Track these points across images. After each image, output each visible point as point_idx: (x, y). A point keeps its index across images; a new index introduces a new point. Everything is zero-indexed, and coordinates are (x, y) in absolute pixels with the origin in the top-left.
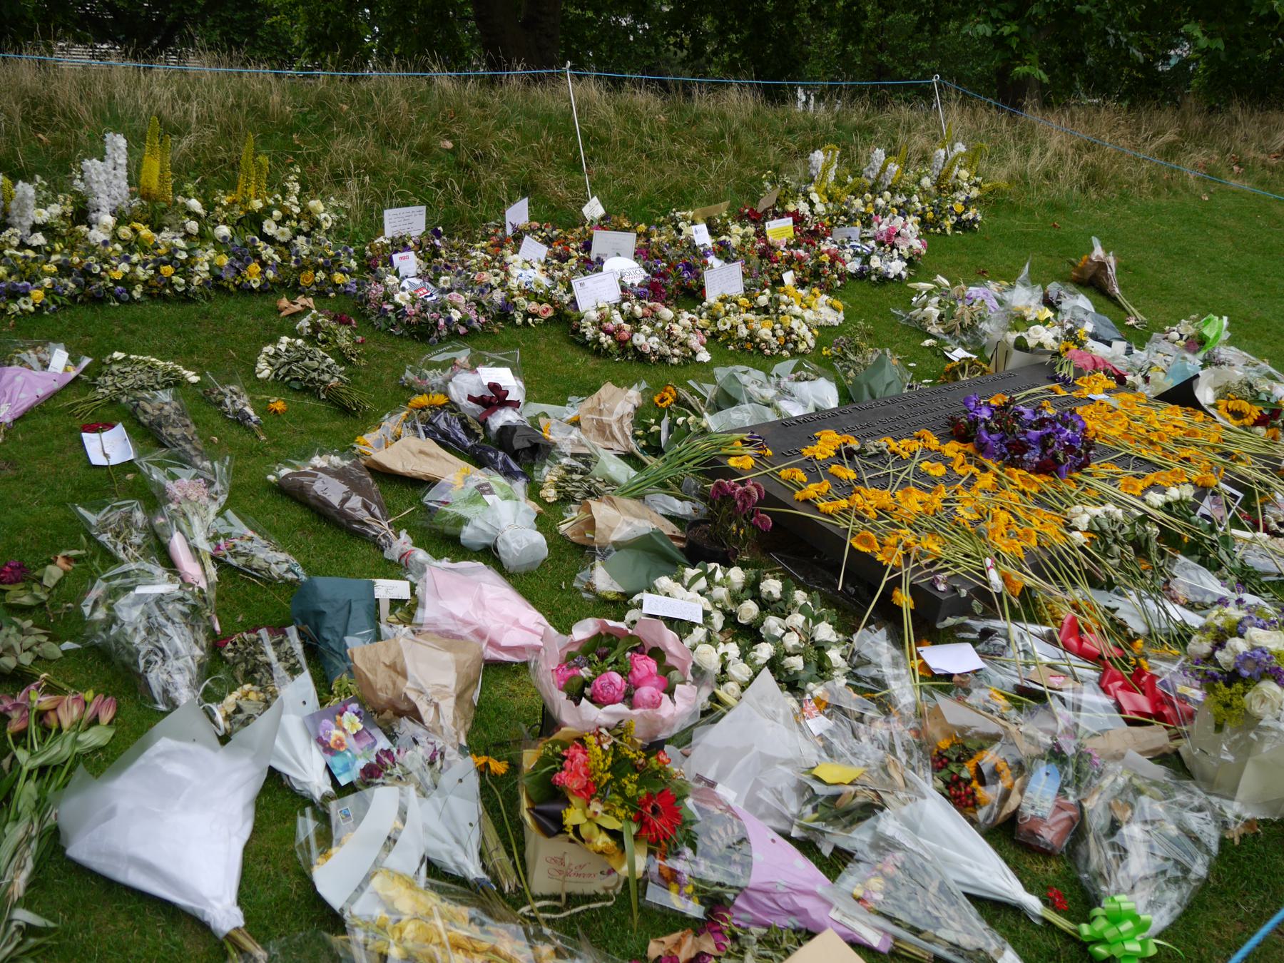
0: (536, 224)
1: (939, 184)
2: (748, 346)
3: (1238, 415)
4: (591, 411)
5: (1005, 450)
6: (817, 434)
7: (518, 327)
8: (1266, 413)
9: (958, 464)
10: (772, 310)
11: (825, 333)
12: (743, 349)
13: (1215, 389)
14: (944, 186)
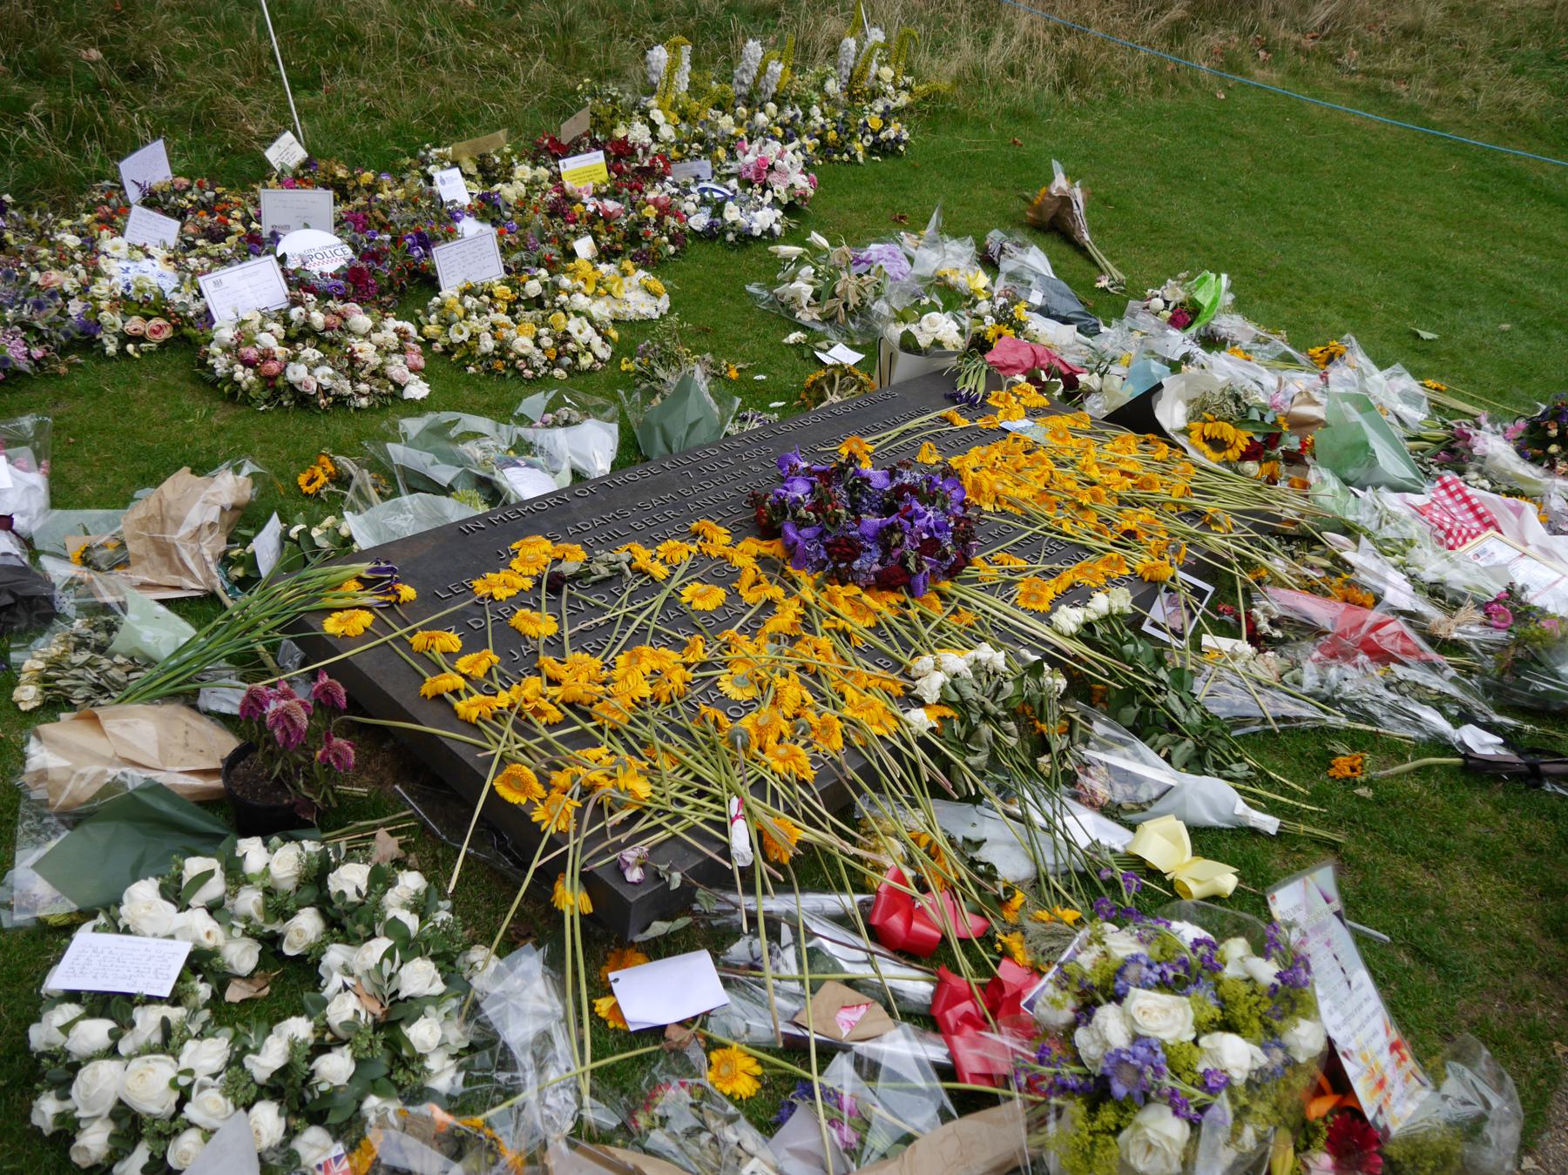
0: (184, 181)
1: (852, 86)
2: (499, 365)
3: (1217, 444)
4: (144, 523)
5: (823, 555)
6: (515, 546)
7: (110, 359)
8: (1258, 439)
9: (746, 584)
10: (547, 303)
11: (631, 331)
12: (490, 371)
13: (1189, 402)
14: (859, 91)
